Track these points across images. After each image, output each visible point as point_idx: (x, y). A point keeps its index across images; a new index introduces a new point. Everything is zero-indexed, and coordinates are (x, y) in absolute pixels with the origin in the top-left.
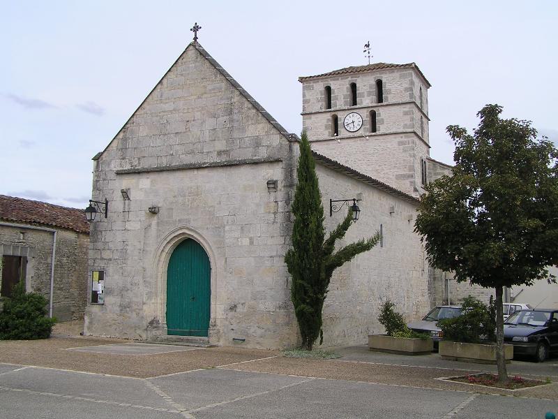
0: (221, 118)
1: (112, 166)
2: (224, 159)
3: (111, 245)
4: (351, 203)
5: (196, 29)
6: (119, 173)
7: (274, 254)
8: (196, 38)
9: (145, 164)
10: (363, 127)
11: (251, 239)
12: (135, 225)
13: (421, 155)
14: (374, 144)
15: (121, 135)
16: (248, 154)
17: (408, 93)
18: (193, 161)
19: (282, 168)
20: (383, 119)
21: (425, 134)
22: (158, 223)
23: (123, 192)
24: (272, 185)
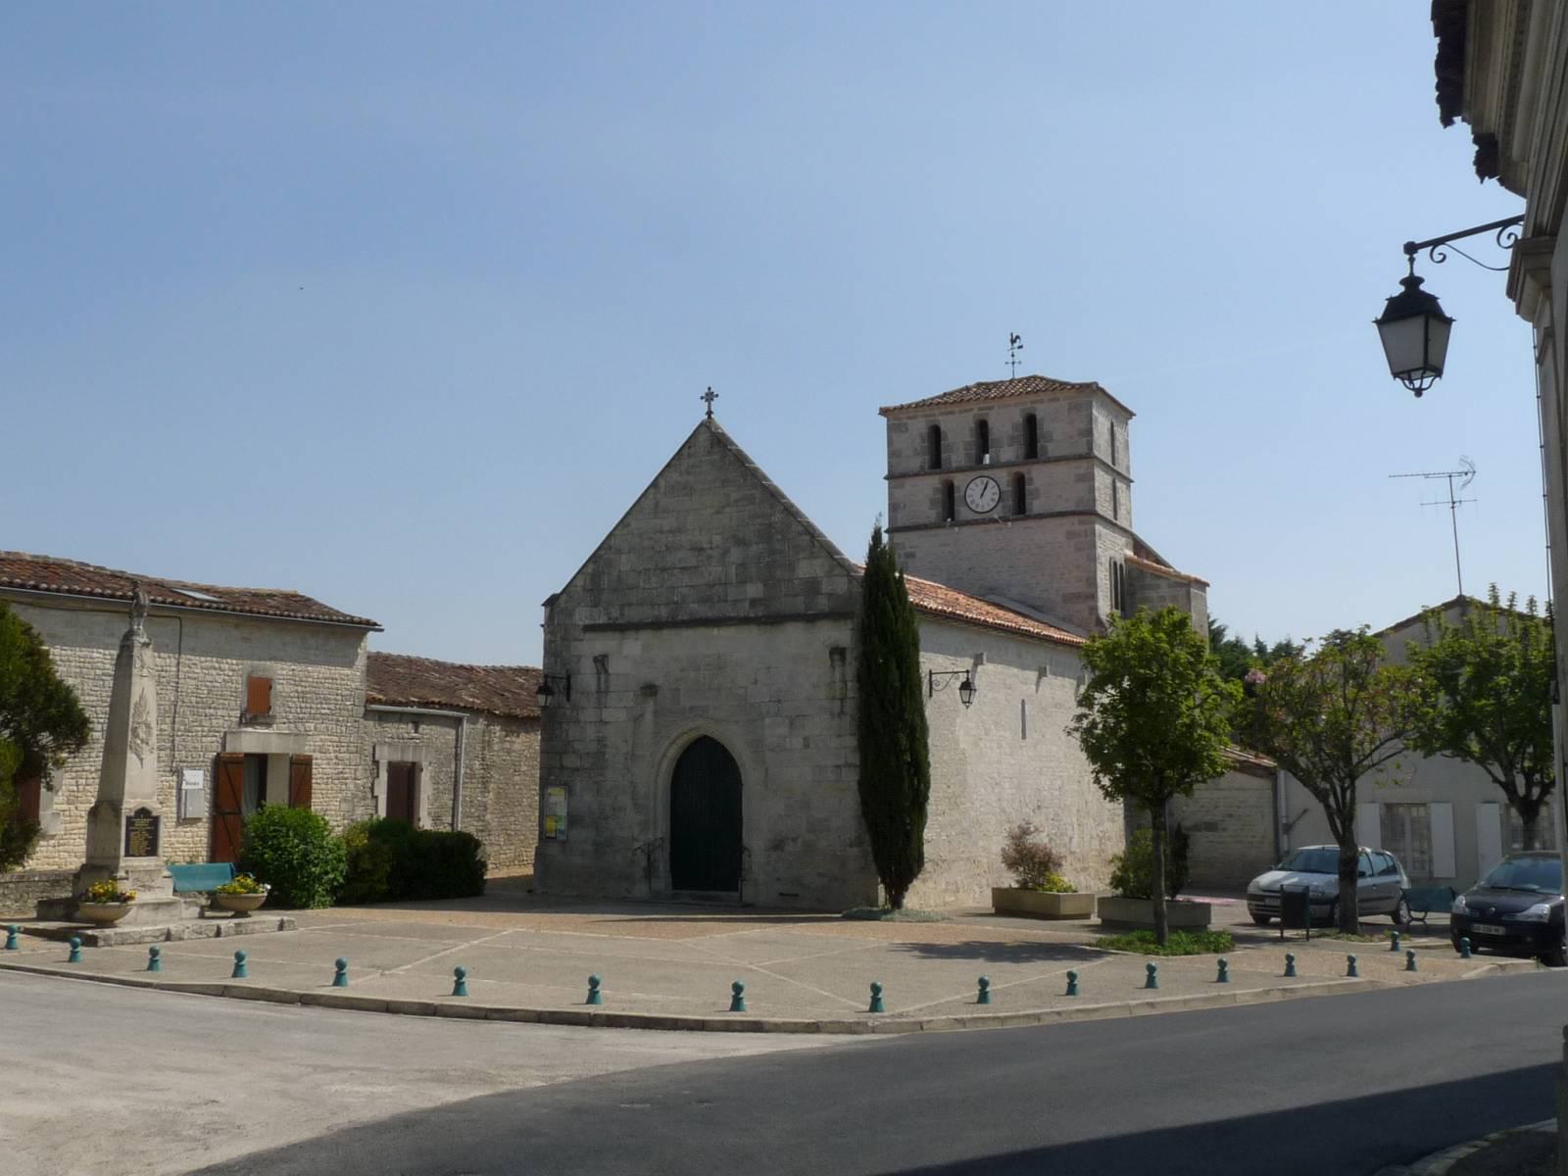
0: (754, 548)
1: (577, 617)
2: (760, 611)
3: (577, 746)
4: (963, 678)
5: (710, 397)
6: (588, 629)
7: (841, 762)
8: (709, 413)
9: (634, 614)
10: (1001, 504)
11: (806, 739)
12: (616, 714)
13: (1111, 553)
14: (1020, 534)
15: (590, 569)
16: (799, 604)
17: (1084, 440)
18: (710, 614)
19: (853, 629)
20: (1037, 490)
21: (1122, 512)
22: (655, 712)
23: (596, 660)
24: (838, 652)
